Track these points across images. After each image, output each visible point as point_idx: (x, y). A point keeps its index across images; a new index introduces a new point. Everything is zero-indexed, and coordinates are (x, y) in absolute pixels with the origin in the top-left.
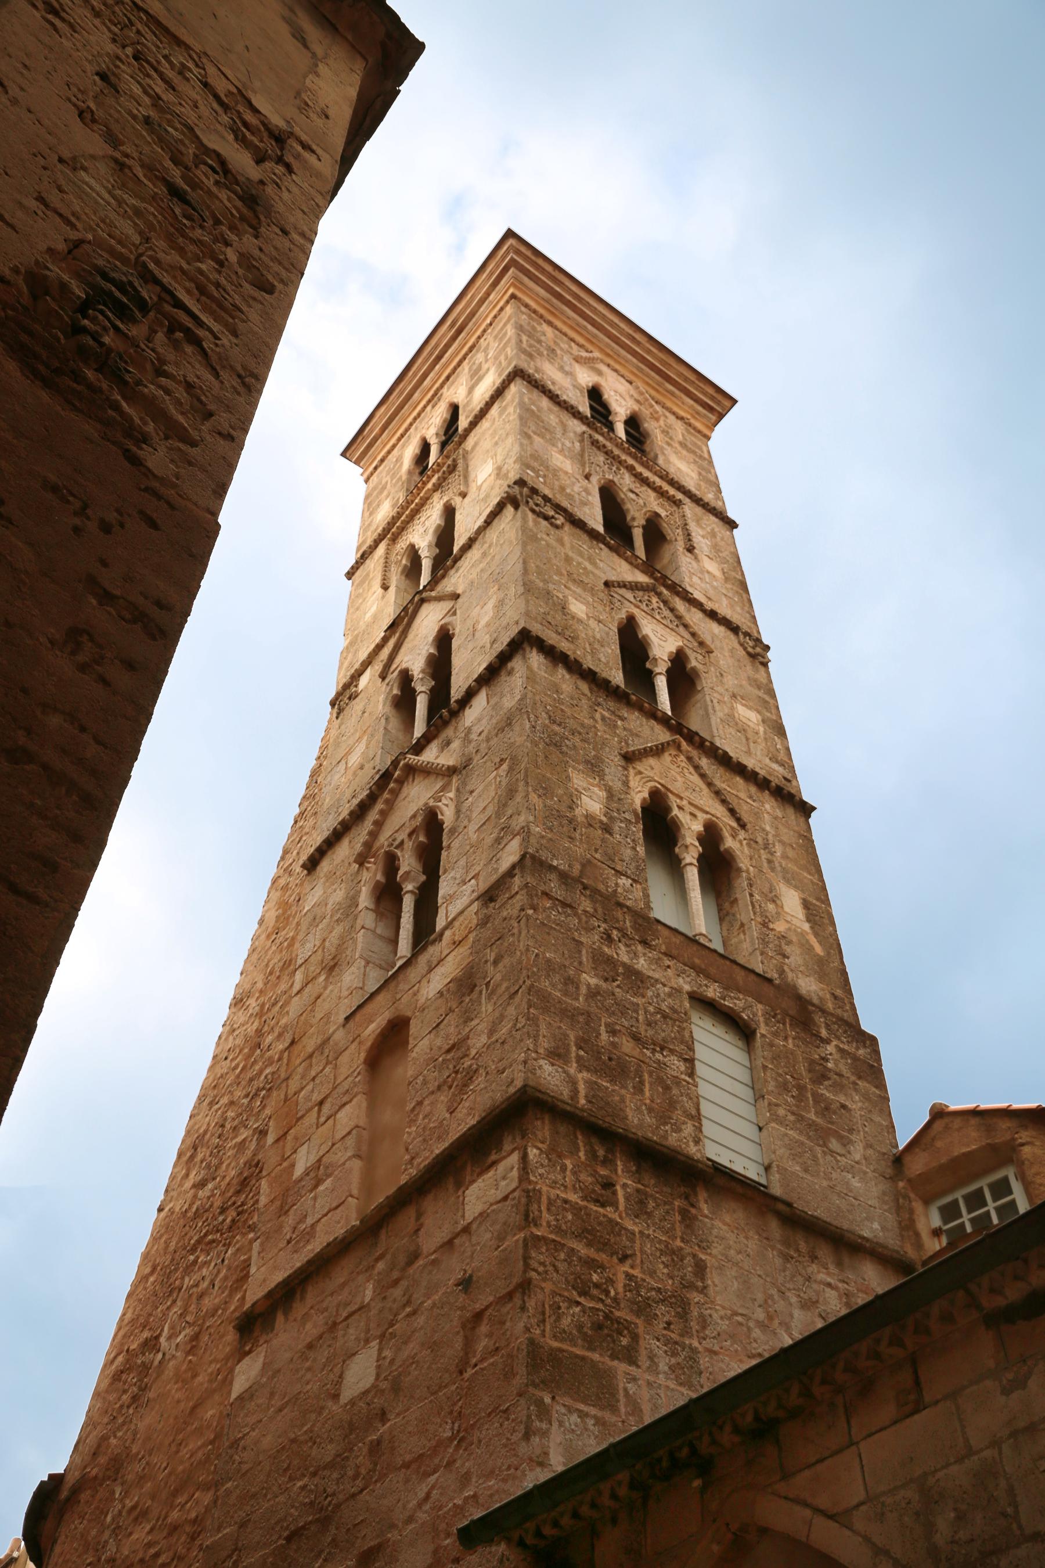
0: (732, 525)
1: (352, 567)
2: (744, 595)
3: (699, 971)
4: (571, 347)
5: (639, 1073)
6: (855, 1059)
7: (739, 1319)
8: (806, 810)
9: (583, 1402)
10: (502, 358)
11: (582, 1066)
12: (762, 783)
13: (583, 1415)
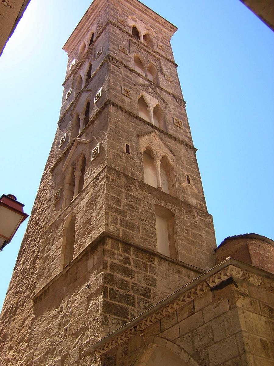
0: (176, 66)
1: (64, 83)
2: (179, 87)
3: (158, 198)
4: (127, 14)
5: (139, 227)
6: (205, 221)
7: (166, 294)
8: (195, 150)
9: (118, 316)
10: (106, 18)
11: (121, 225)
12: (182, 142)
13: (118, 320)
